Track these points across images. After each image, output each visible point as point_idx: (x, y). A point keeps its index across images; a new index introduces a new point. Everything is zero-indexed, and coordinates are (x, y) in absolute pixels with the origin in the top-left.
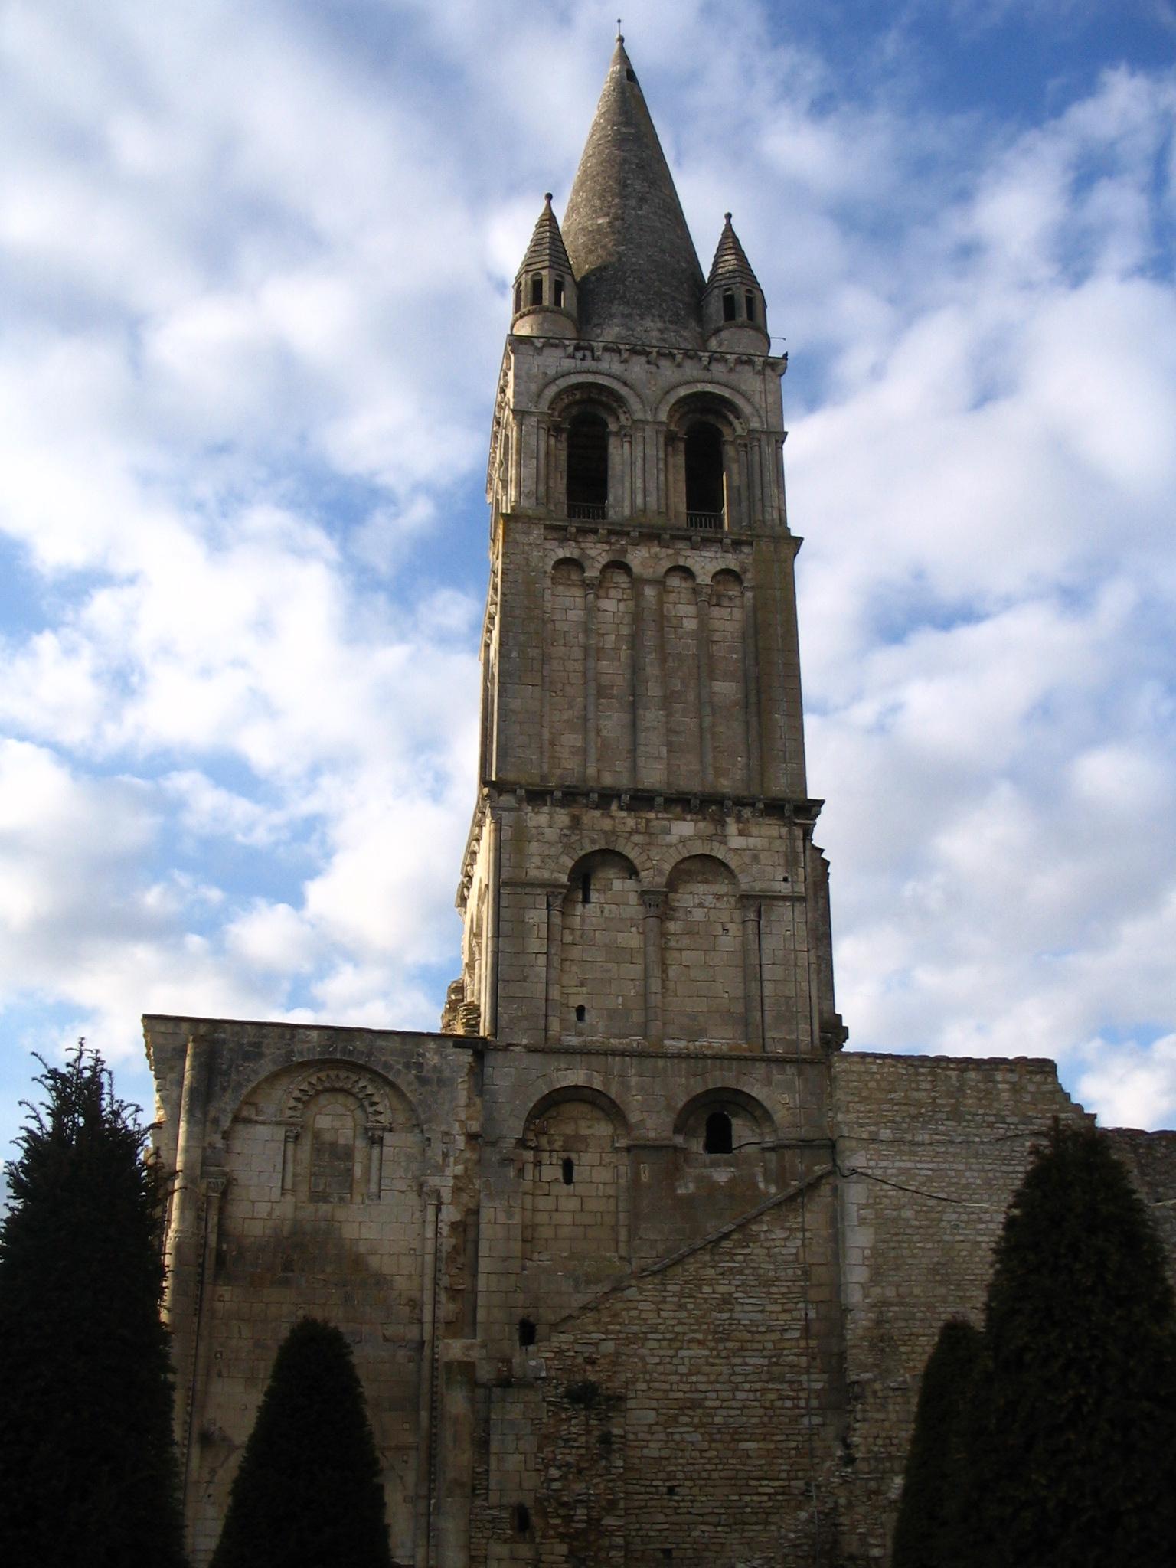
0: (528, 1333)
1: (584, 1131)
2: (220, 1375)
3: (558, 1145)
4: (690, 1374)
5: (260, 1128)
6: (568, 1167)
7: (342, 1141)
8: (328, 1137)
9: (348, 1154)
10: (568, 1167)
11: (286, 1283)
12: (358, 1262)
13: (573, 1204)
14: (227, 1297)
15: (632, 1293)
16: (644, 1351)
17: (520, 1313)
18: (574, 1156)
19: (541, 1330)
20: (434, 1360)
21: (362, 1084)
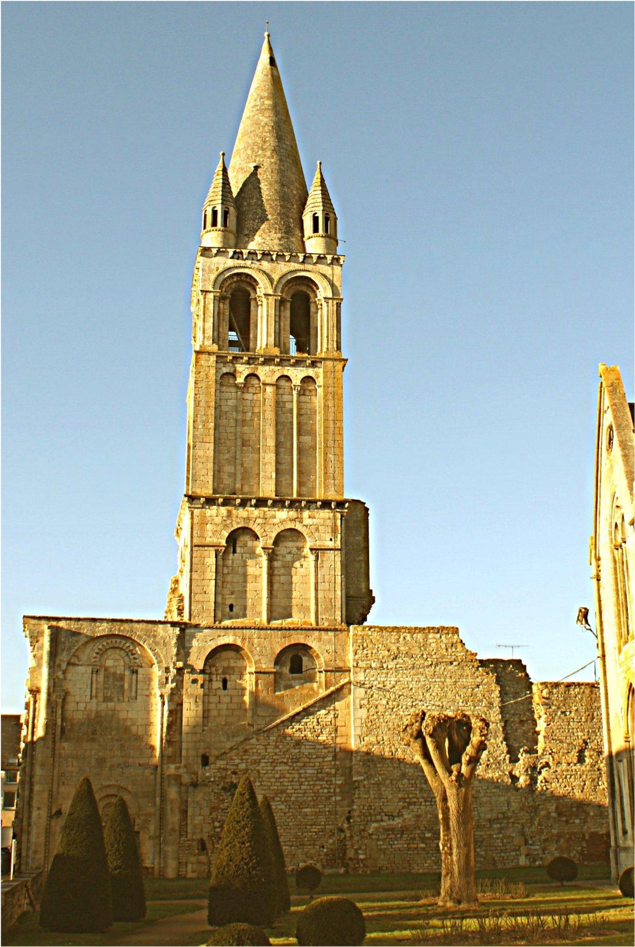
0: (205, 761)
1: (232, 665)
2: (63, 783)
3: (220, 671)
4: (280, 778)
5: (80, 668)
6: (225, 682)
7: (118, 672)
8: (112, 670)
9: (122, 678)
10: (225, 682)
11: (93, 740)
12: (127, 729)
13: (227, 699)
14: (66, 747)
15: (254, 741)
16: (259, 768)
17: (201, 752)
18: (228, 677)
19: (212, 759)
20: (162, 774)
21: (128, 645)
